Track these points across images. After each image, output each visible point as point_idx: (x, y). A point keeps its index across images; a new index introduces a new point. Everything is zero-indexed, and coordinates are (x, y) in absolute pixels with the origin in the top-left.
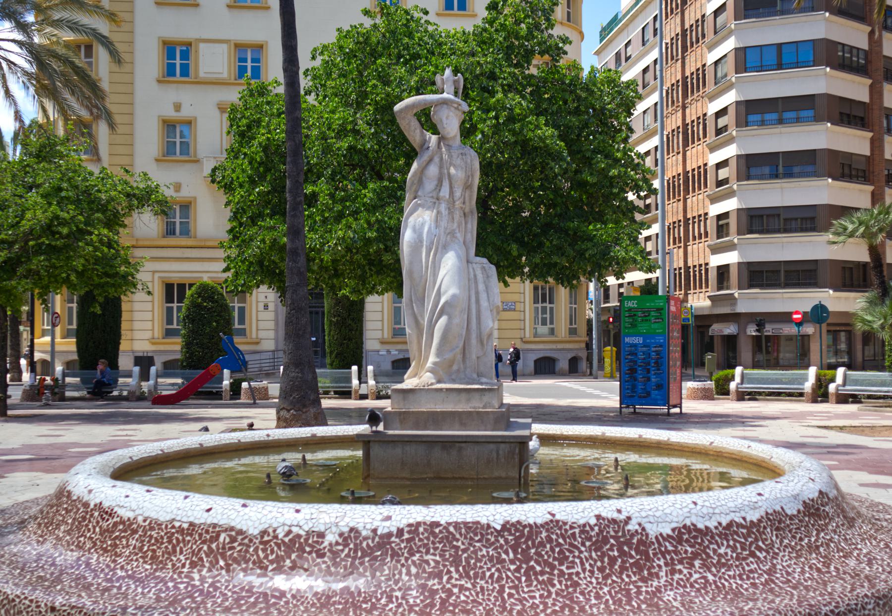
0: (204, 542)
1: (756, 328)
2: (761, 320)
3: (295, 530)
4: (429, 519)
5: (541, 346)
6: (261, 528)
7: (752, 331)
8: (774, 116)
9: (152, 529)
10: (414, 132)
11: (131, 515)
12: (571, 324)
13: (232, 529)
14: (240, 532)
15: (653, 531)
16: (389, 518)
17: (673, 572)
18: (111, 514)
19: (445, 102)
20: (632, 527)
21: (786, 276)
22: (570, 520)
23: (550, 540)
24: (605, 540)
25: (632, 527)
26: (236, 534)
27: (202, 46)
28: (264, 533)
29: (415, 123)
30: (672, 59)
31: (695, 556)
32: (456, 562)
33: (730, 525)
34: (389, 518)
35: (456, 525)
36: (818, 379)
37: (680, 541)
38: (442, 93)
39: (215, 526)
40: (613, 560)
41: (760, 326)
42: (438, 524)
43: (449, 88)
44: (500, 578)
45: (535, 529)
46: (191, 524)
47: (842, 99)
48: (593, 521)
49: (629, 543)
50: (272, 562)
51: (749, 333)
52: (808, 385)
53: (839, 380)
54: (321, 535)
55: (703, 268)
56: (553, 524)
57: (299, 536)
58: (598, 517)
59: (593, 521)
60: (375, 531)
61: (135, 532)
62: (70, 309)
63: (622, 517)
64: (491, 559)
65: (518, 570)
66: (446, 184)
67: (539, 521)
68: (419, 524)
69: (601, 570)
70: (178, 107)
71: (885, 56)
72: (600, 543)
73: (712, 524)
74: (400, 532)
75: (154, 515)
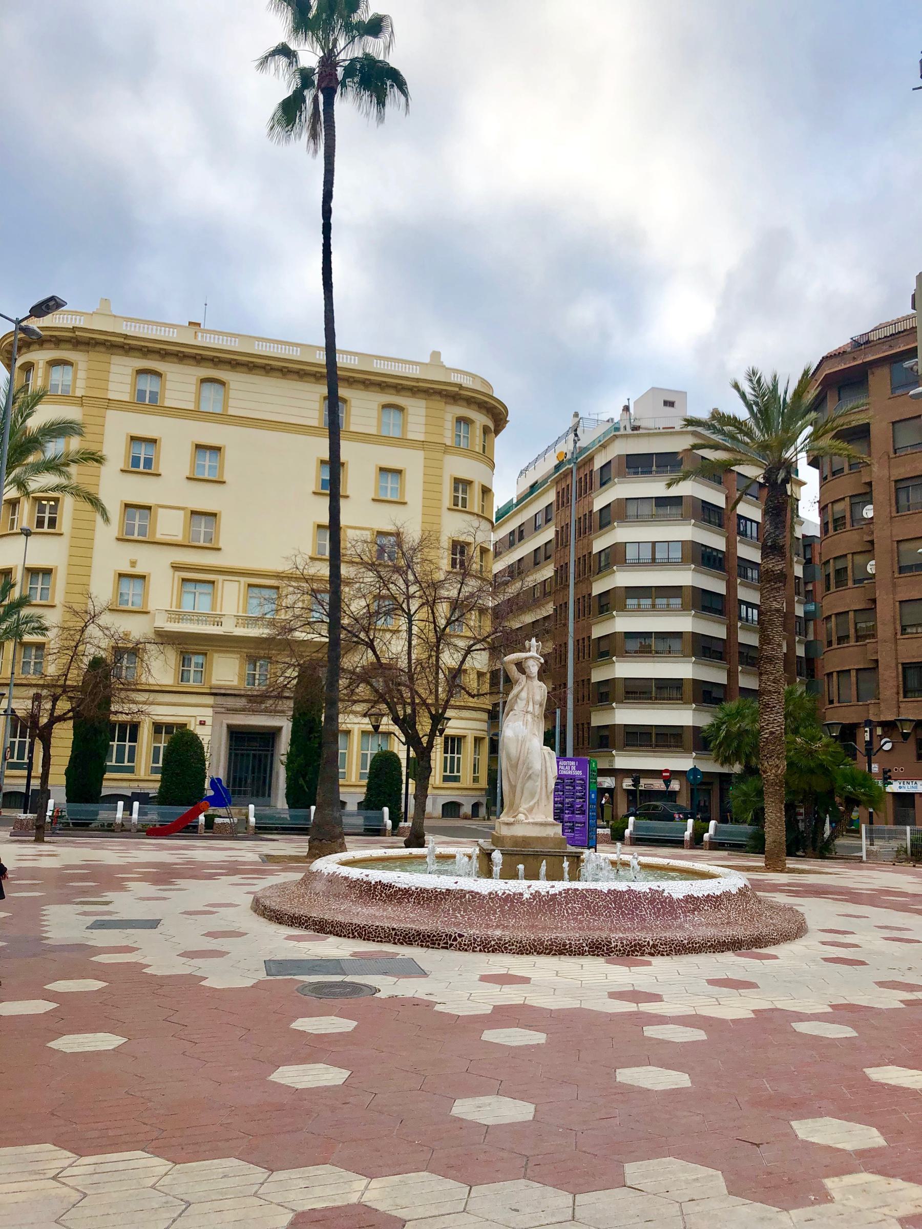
0: (457, 899)
1: (631, 783)
2: (637, 775)
3: (507, 892)
4: (573, 887)
5: (448, 792)
6: (489, 891)
7: (627, 783)
8: (648, 602)
9: (423, 893)
10: (514, 671)
11: (407, 887)
12: (474, 773)
13: (472, 892)
14: (477, 893)
15: (675, 896)
16: (553, 887)
17: (686, 916)
18: (391, 886)
19: (532, 657)
20: (665, 894)
21: (656, 738)
22: (638, 889)
23: (630, 899)
24: (655, 900)
25: (665, 894)
26: (474, 895)
27: (160, 510)
28: (490, 893)
29: (515, 668)
30: (562, 545)
31: (695, 910)
32: (589, 908)
33: (708, 895)
34: (553, 887)
35: (587, 890)
36: (694, 829)
37: (687, 902)
38: (529, 650)
39: (462, 890)
40: (659, 909)
41: (636, 782)
42: (578, 890)
43: (534, 649)
44: (610, 916)
45: (622, 893)
46: (447, 890)
47: (704, 591)
48: (648, 891)
49: (665, 901)
50: (498, 908)
51: (625, 787)
52: (688, 834)
53: (711, 830)
54: (521, 894)
55: (586, 726)
56: (630, 891)
57: (509, 895)
58: (650, 889)
59: (648, 891)
60: (548, 892)
61: (412, 895)
62: (13, 743)
63: (661, 889)
64: (604, 907)
65: (617, 912)
66: (531, 704)
67: (624, 890)
68: (569, 890)
69: (655, 914)
70: (133, 564)
71: (739, 557)
72: (652, 901)
73: (700, 895)
74: (560, 893)
75: (423, 886)
